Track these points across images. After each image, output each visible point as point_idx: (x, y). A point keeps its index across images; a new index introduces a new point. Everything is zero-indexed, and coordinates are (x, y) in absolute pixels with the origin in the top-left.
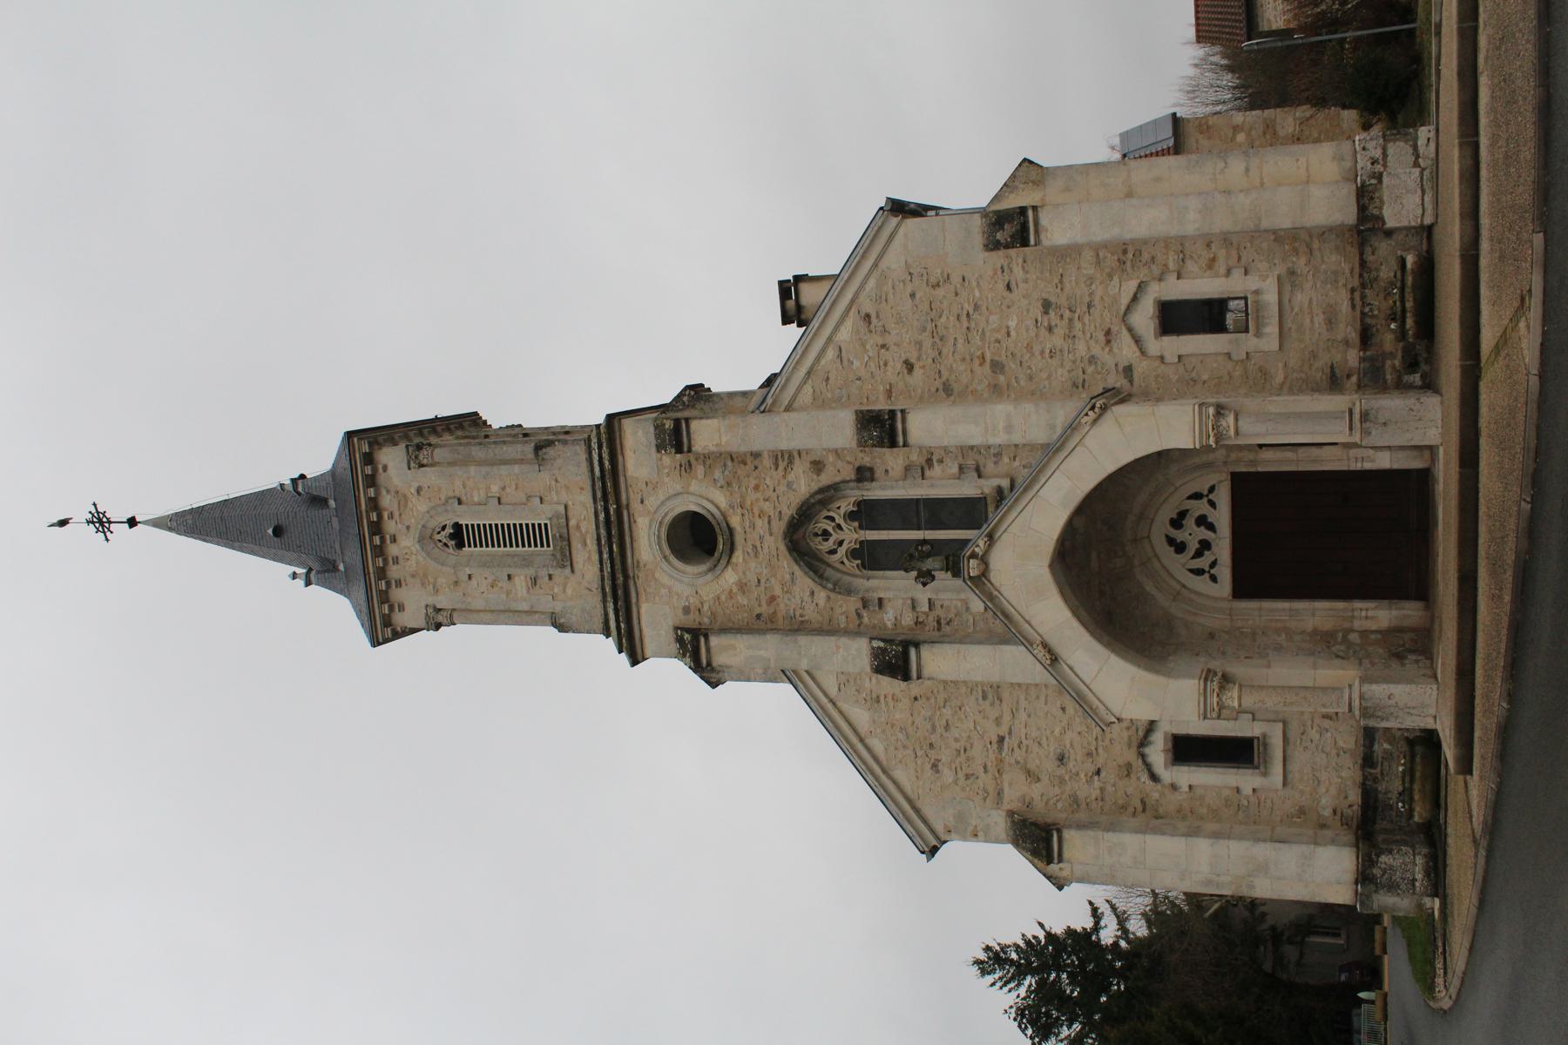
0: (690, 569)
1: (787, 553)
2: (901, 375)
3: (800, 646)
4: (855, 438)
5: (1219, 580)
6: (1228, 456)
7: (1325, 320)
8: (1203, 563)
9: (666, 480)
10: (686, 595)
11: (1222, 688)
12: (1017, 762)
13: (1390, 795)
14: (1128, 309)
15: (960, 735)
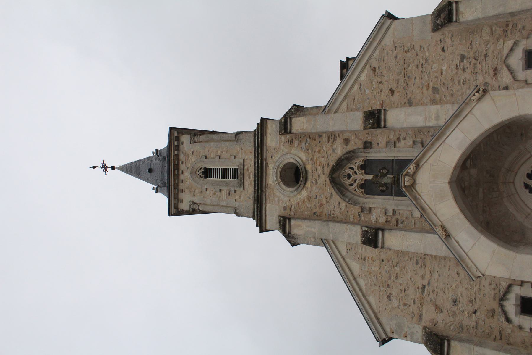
2: (388, 96)
4: (363, 125)
12: (431, 300)
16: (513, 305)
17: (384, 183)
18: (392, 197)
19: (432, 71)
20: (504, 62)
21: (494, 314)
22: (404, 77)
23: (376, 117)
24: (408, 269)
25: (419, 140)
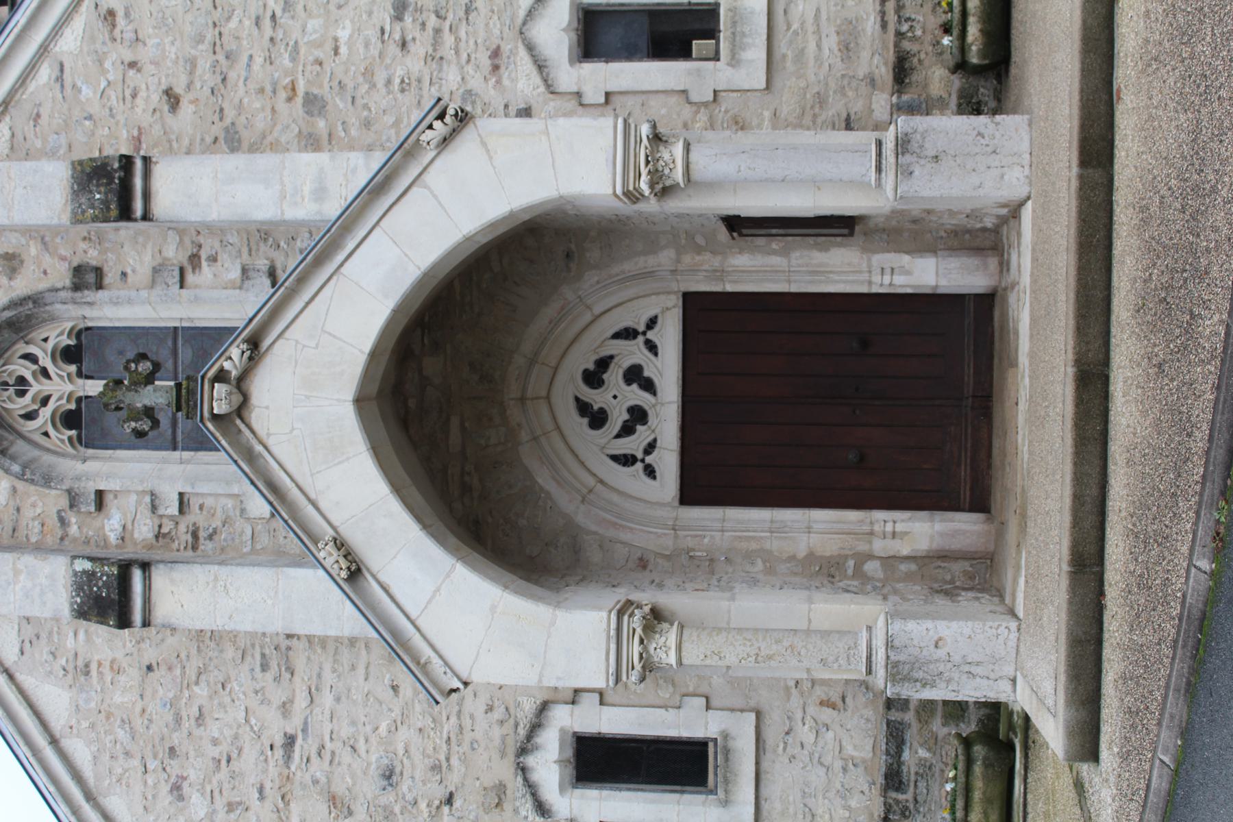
2: (158, 113)
4: (69, 208)
5: (658, 474)
6: (678, 261)
7: (839, 43)
8: (633, 445)
11: (649, 629)
12: (316, 782)
16: (555, 762)
17: (145, 407)
18: (177, 454)
19: (306, 40)
20: (521, 33)
21: (503, 796)
22: (215, 53)
23: (117, 181)
24: (237, 688)
25: (262, 264)
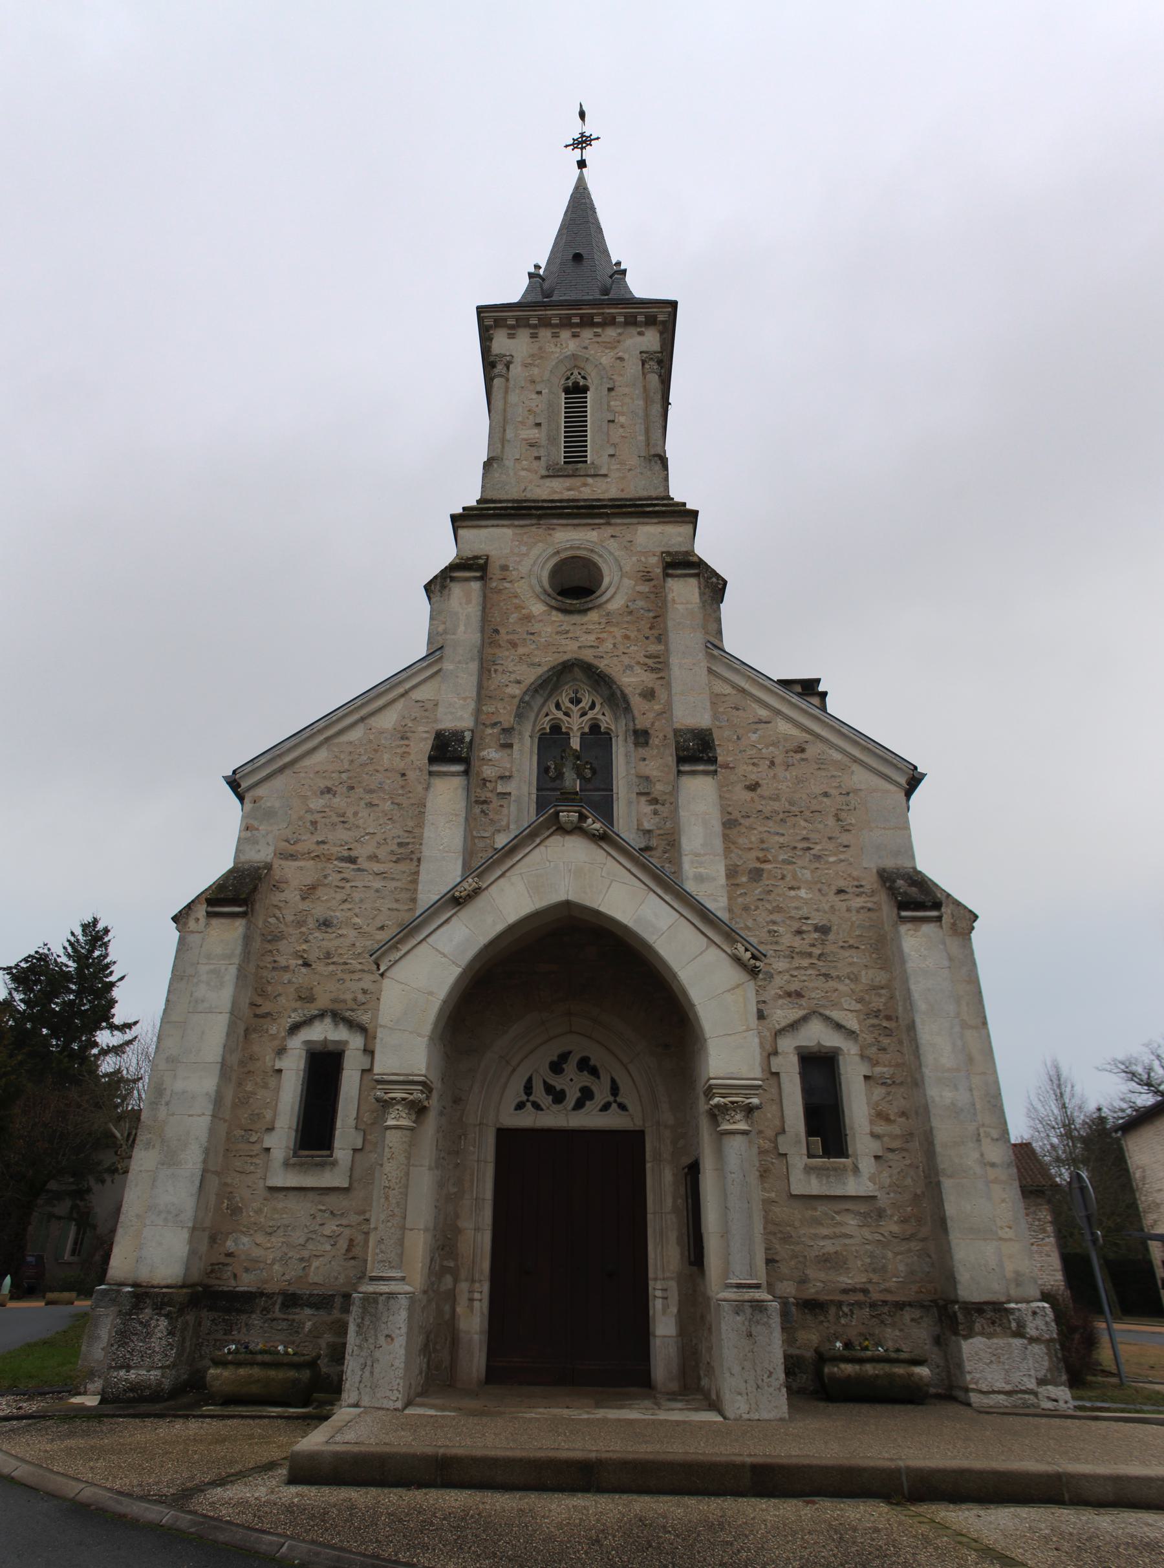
0: (545, 575)
1: (561, 660)
3: (467, 663)
5: (518, 1112)
7: (829, 1254)
8: (539, 1094)
9: (634, 559)
10: (520, 568)
12: (325, 877)
13: (244, 1330)
14: (827, 1019)
15: (361, 818)
